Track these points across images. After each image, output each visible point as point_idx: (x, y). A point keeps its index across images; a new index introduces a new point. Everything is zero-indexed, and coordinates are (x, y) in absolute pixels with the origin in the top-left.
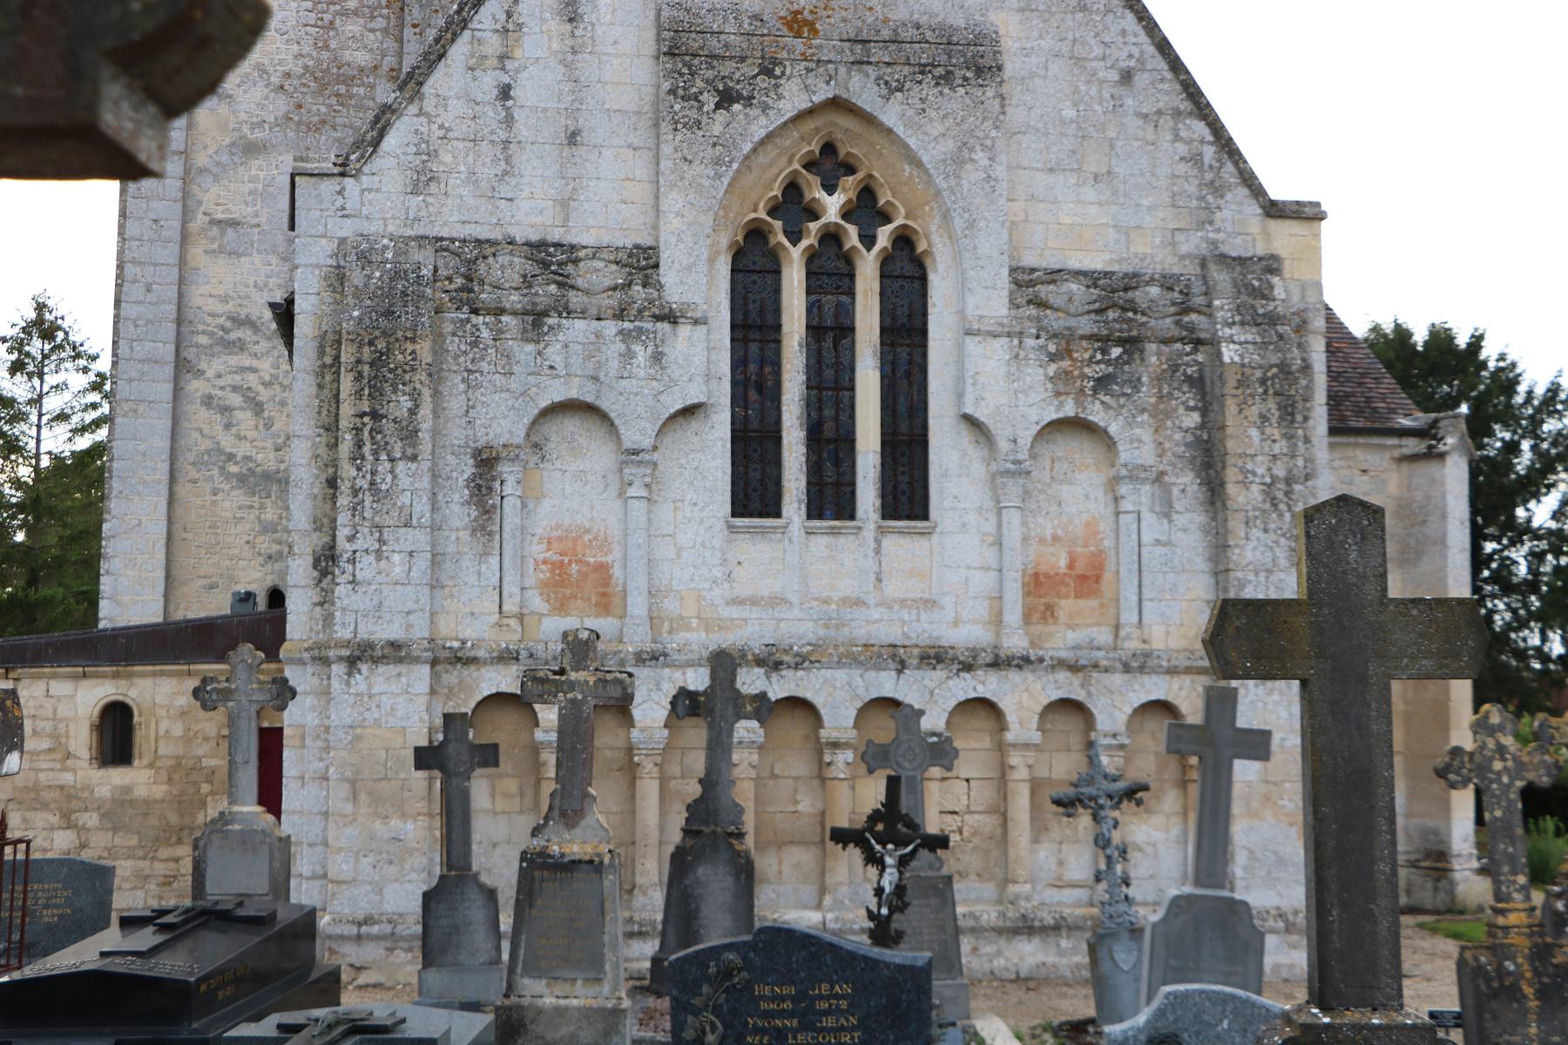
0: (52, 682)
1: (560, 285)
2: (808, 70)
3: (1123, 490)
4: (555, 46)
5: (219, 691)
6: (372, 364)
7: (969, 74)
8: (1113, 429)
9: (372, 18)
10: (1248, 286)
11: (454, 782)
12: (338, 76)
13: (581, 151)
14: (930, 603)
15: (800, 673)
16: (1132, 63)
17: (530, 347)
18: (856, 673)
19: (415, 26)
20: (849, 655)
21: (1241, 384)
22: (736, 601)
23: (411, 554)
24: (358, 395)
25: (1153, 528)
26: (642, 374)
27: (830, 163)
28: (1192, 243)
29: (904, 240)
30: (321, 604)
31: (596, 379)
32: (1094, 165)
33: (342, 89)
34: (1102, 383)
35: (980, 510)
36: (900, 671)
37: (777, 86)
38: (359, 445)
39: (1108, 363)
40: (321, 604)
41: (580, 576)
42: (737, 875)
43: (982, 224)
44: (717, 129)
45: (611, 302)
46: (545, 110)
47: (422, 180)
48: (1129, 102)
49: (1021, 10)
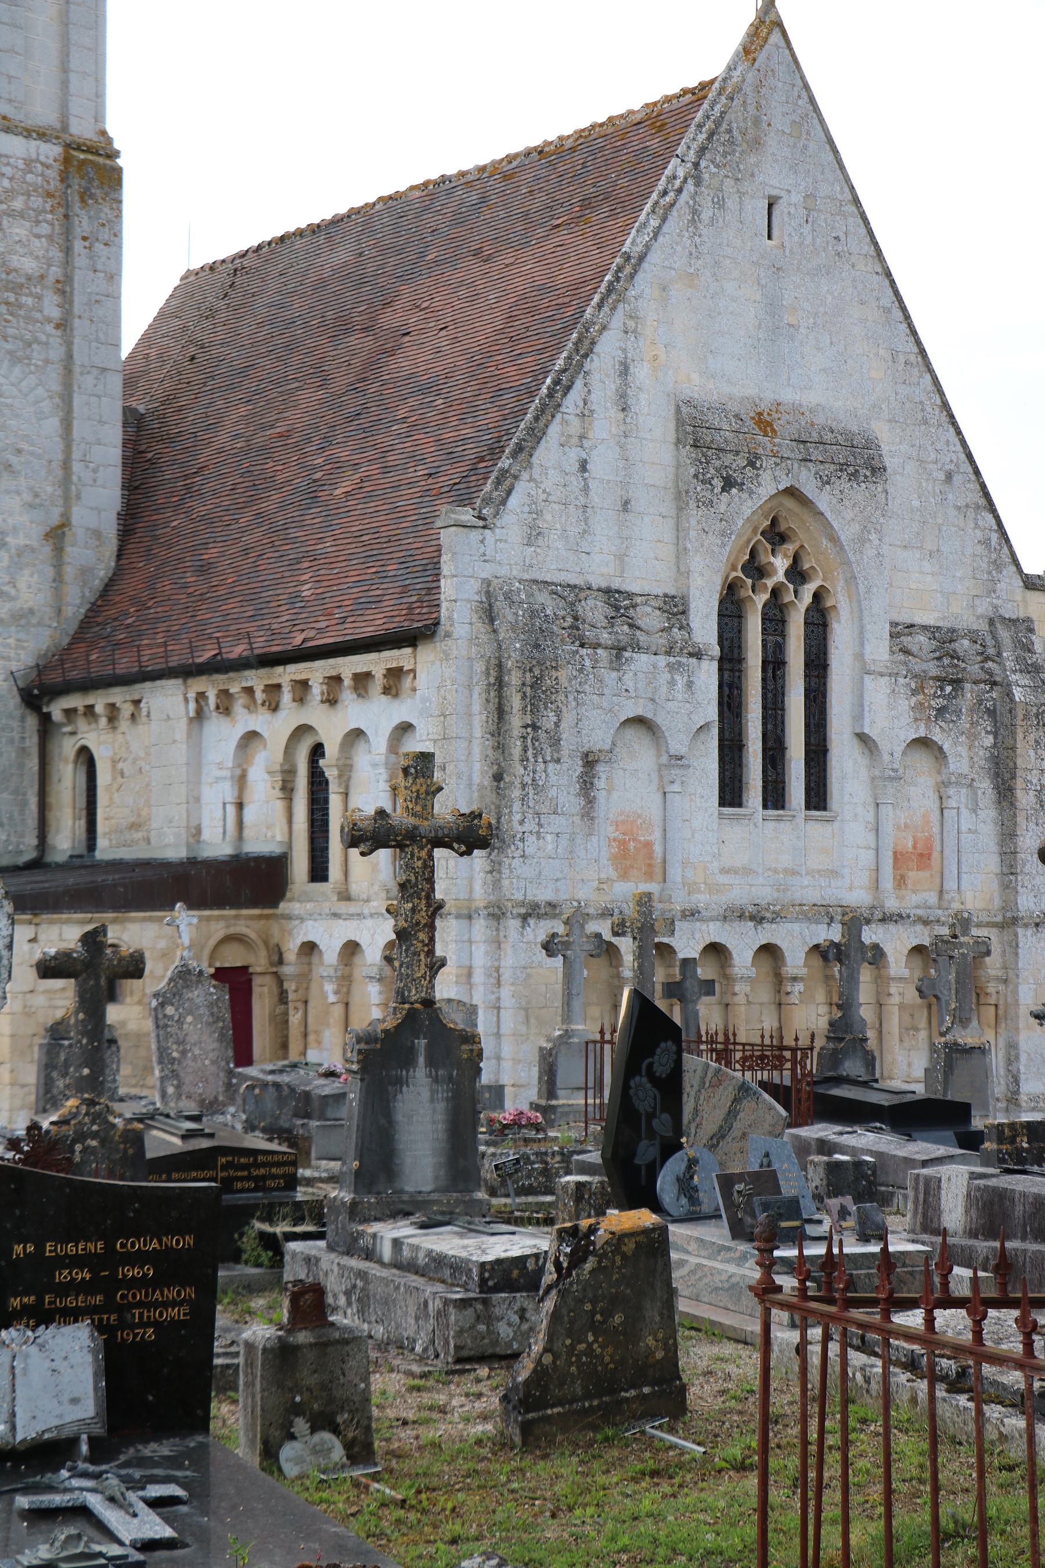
0: (65, 927)
1: (631, 626)
2: (777, 464)
3: (951, 791)
4: (614, 430)
5: (563, 943)
6: (532, 687)
7: (868, 473)
8: (946, 747)
9: (38, 222)
10: (1020, 641)
11: (690, 1006)
12: (8, 282)
13: (630, 516)
14: (834, 873)
15: (774, 926)
16: (952, 467)
17: (614, 674)
18: (804, 925)
19: (85, 239)
20: (803, 913)
21: (1026, 717)
22: (724, 871)
23: (557, 835)
24: (524, 710)
25: (967, 820)
26: (680, 698)
27: (776, 535)
28: (984, 607)
29: (818, 596)
30: (491, 872)
31: (653, 700)
32: (929, 546)
33: (12, 297)
34: (941, 711)
35: (864, 805)
36: (829, 924)
37: (758, 475)
38: (525, 750)
39: (944, 697)
40: (491, 872)
41: (633, 854)
42: (867, 1067)
43: (875, 590)
44: (723, 508)
45: (661, 641)
46: (609, 481)
47: (534, 535)
48: (950, 496)
49: (890, 421)
